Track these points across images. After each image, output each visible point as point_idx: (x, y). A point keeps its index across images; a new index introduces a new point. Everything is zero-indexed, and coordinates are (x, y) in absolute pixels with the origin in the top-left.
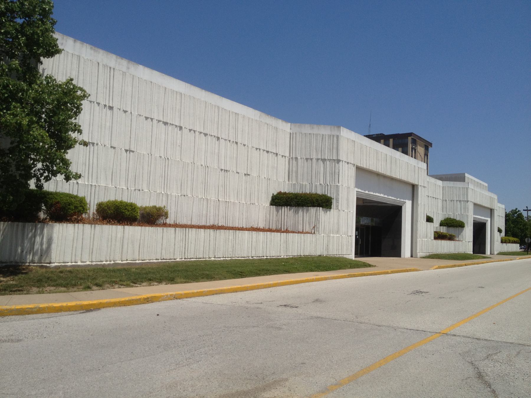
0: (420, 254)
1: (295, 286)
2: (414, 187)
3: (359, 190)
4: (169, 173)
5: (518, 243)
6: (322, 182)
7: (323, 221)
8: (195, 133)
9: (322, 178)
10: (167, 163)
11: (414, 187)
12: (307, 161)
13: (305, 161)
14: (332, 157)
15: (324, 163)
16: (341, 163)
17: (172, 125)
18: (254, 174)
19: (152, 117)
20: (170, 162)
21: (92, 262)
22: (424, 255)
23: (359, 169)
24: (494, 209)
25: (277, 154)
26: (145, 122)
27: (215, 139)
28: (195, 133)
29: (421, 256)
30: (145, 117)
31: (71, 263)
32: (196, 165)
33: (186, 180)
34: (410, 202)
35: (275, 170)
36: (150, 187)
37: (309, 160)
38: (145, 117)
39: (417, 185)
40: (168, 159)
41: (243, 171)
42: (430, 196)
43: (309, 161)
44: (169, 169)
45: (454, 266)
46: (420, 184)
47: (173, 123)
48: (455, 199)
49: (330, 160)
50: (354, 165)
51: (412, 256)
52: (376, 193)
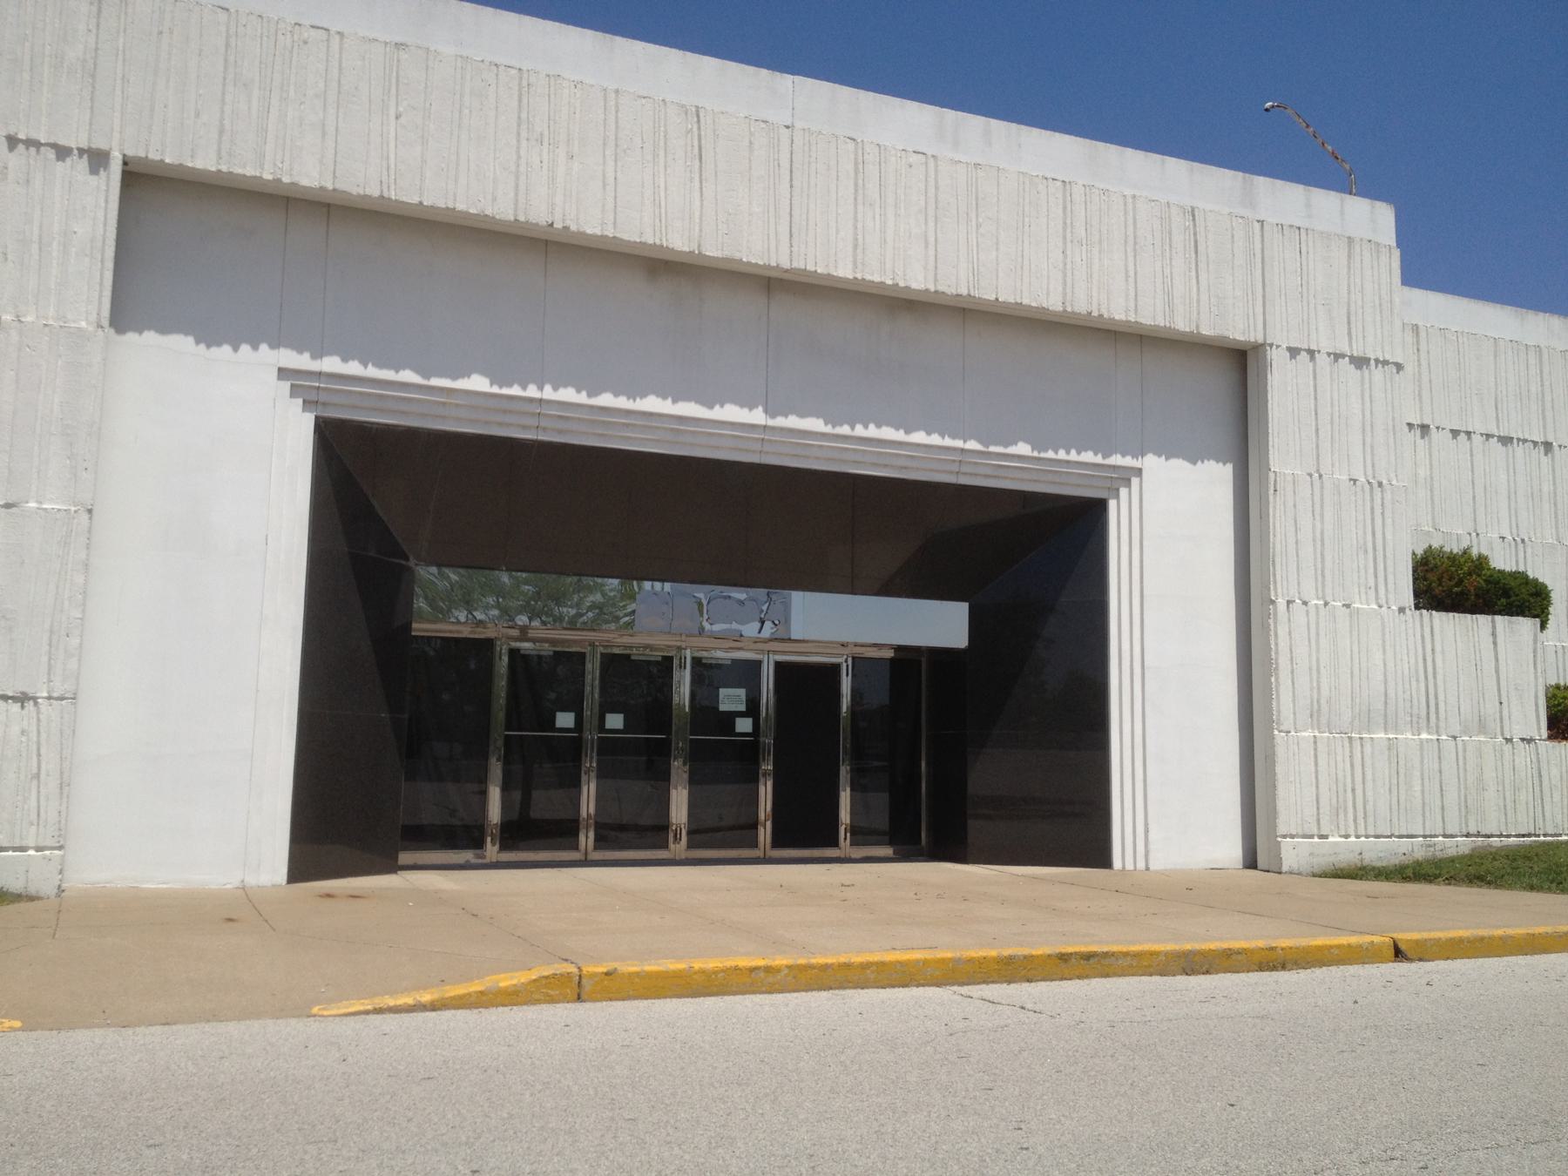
0: (1294, 854)
1: (389, 1016)
2: (1241, 363)
4: (1389, 536)
5: (416, 637)
8: (1312, 358)
10: (1378, 501)
11: (1241, 363)
17: (1385, 363)
19: (1314, 347)
20: (1388, 496)
22: (1343, 846)
26: (1291, 365)
28: (1312, 358)
29: (1323, 861)
30: (1290, 349)
32: (1327, 484)
33: (1291, 541)
36: (1328, 591)
38: (1290, 349)
39: (1259, 348)
40: (1380, 484)
44: (1389, 521)
46: (1281, 336)
47: (1387, 357)
50: (97, 159)
51: (1251, 862)
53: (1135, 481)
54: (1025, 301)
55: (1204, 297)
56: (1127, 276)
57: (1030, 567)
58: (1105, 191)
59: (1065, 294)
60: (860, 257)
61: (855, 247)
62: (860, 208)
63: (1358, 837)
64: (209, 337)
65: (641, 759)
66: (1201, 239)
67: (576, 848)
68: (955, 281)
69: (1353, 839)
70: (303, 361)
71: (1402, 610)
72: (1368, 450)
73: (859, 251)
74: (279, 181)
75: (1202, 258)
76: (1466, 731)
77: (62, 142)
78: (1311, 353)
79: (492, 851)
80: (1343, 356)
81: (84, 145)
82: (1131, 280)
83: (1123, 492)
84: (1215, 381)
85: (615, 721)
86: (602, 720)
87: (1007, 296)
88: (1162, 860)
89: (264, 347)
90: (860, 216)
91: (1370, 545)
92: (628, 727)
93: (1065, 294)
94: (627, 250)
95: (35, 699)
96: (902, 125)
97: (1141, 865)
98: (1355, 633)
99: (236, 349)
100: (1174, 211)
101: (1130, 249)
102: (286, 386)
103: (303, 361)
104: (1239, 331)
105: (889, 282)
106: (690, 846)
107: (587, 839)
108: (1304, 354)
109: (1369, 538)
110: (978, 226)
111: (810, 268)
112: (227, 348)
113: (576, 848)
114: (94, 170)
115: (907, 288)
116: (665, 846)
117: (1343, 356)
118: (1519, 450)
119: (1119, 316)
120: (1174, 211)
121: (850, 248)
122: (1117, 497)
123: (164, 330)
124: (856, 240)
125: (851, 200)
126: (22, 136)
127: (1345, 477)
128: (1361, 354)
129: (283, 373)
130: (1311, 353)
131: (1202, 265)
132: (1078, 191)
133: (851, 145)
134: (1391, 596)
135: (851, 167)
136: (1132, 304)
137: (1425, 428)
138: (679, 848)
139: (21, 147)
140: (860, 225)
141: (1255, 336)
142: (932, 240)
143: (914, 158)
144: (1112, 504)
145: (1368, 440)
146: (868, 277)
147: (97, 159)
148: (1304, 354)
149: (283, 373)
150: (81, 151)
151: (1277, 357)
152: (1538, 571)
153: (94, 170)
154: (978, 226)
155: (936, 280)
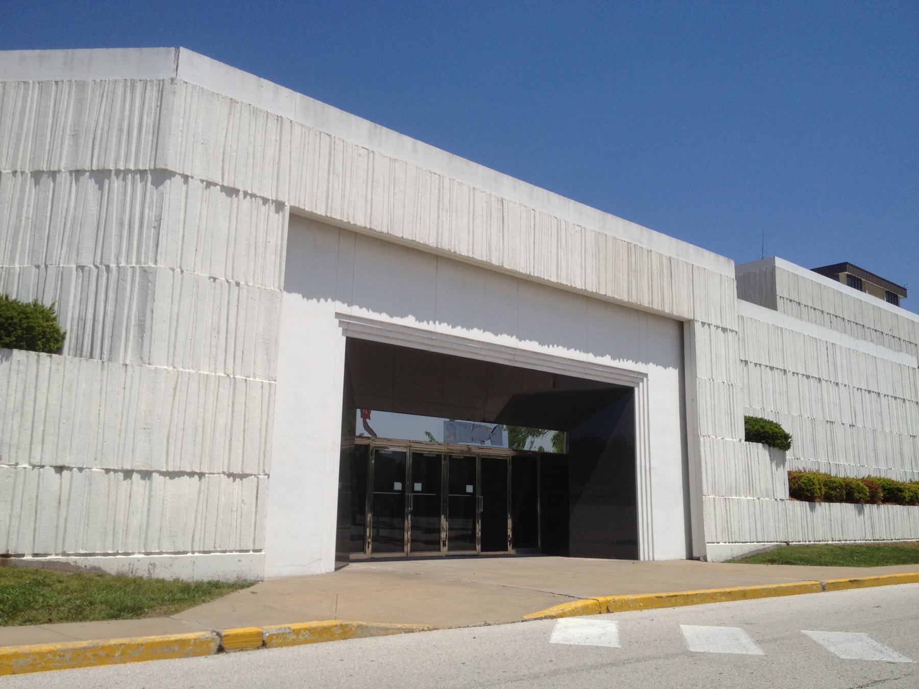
2: (682, 327)
3: (357, 311)
6: (87, 261)
7: (709, 466)
9: (88, 243)
11: (682, 327)
12: (37, 183)
13: (30, 181)
14: (136, 164)
15: (101, 188)
16: (173, 186)
17: (253, 196)
18: (860, 425)
20: (244, 293)
21: (64, 554)
23: (300, 221)
24: (691, 322)
25: (785, 371)
27: (782, 373)
31: (193, 552)
34: (672, 374)
35: (785, 398)
37: (44, 178)
39: (691, 322)
40: (238, 284)
41: (848, 421)
42: (752, 359)
43: (47, 182)
44: (242, 312)
45: (855, 583)
46: (700, 317)
48: (64, 164)
49: (127, 171)
50: (279, 206)
51: (690, 557)
52: (469, 327)
53: (645, 379)
54: (418, 240)
55: (506, 249)
56: (469, 232)
57: (598, 418)
58: (460, 184)
59: (438, 238)
60: (330, 203)
61: (327, 198)
62: (331, 176)
63: (193, 552)
64: (308, 295)
65: (427, 508)
66: (506, 217)
67: (403, 551)
68: (381, 225)
69: (721, 544)
70: (344, 309)
71: (740, 440)
72: (230, 257)
73: (330, 200)
74: (349, 223)
75: (506, 226)
76: (762, 496)
77: (266, 196)
78: (709, 325)
79: (511, 550)
80: (216, 185)
81: (274, 198)
82: (369, 203)
83: (641, 384)
84: (672, 332)
85: (418, 487)
86: (413, 487)
87: (408, 236)
88: (658, 557)
89: (322, 300)
90: (331, 180)
91: (223, 328)
92: (424, 489)
93: (438, 238)
94: (406, 245)
95: (70, 469)
96: (354, 132)
97: (651, 559)
98: (728, 455)
99: (319, 301)
100: (493, 199)
101: (471, 217)
102: (337, 321)
103: (344, 309)
104: (683, 312)
105: (345, 220)
106: (449, 550)
107: (407, 548)
108: (178, 177)
109: (223, 322)
110: (394, 194)
111: (302, 207)
112: (315, 300)
113: (403, 551)
114: (277, 211)
115: (355, 225)
116: (439, 550)
117: (216, 185)
118: (776, 371)
119: (464, 253)
120: (493, 199)
121: (324, 198)
122: (638, 387)
123: (531, 340)
124: (328, 193)
125: (326, 171)
126: (249, 192)
127: (207, 275)
128: (231, 186)
129: (338, 315)
130: (709, 325)
131: (506, 229)
132: (447, 181)
133: (328, 139)
134: (238, 369)
135: (327, 151)
136: (471, 248)
137: (746, 362)
138: (444, 550)
139: (248, 197)
140: (330, 185)
141: (690, 317)
142: (369, 198)
143: (362, 151)
144: (636, 389)
145: (231, 250)
146: (334, 216)
147: (279, 206)
148: (178, 177)
149: (338, 315)
150: (273, 201)
151: (698, 326)
152: (786, 428)
153: (277, 211)
154: (394, 194)
155: (371, 223)
